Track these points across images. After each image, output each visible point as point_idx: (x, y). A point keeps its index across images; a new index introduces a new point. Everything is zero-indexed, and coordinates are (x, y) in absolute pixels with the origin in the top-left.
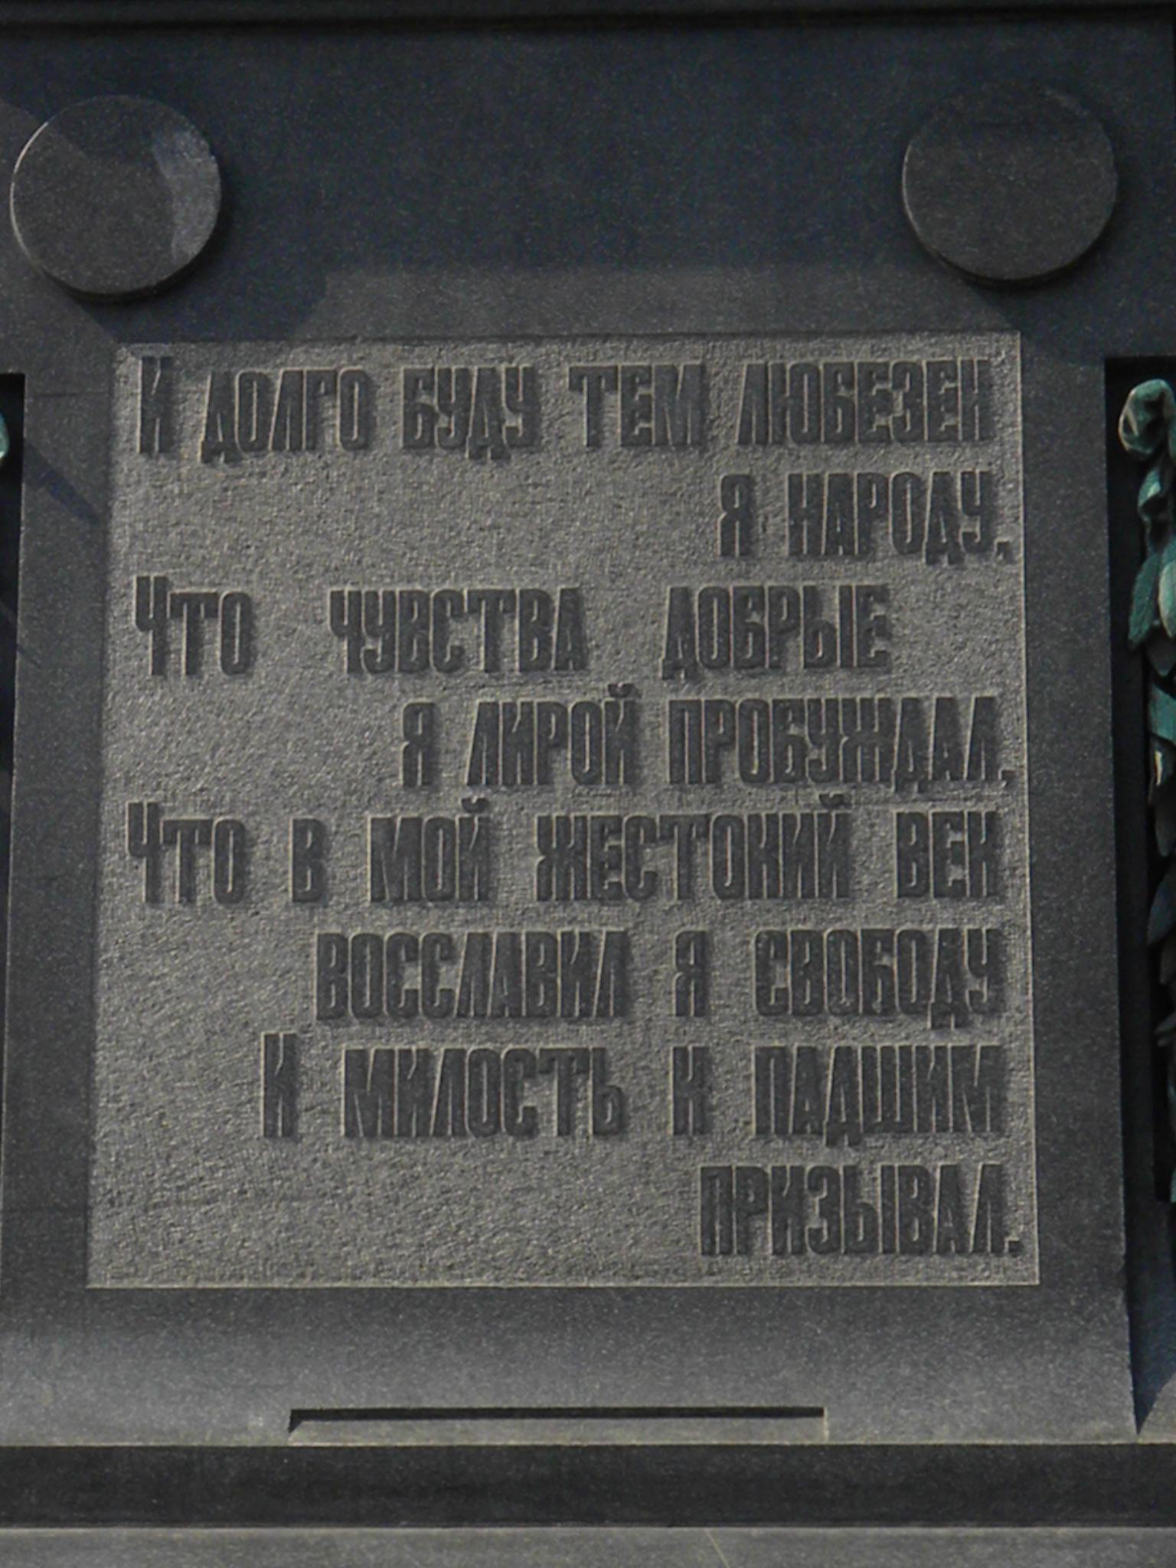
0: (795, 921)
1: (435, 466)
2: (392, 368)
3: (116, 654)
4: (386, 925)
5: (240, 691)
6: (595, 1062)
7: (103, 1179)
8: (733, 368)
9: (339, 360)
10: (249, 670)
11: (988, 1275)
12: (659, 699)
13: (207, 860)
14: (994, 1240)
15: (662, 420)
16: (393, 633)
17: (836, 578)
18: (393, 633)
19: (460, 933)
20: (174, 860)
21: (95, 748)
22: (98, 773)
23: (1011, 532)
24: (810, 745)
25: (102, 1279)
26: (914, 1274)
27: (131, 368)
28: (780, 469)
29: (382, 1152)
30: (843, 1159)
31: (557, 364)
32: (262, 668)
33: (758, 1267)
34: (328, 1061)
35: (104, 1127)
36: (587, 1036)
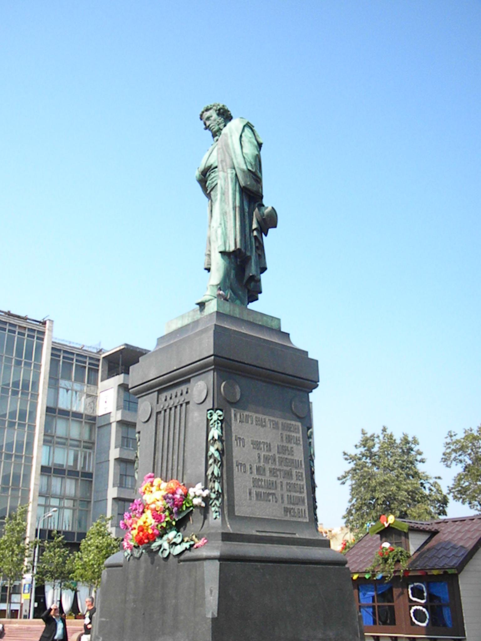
0: (289, 482)
1: (258, 427)
2: (254, 415)
3: (233, 443)
4: (257, 477)
5: (244, 449)
6: (274, 494)
7: (236, 502)
8: (280, 421)
9: (250, 414)
10: (217, 112)
11: (305, 521)
12: (277, 456)
13: (242, 468)
14: (305, 517)
15: (276, 426)
16: (256, 445)
17: (290, 446)
18: (256, 445)
19: (263, 479)
20: (239, 467)
21: (232, 454)
22: (232, 456)
23: (301, 443)
24: (26, 591)
25: (236, 514)
26: (300, 520)
27: (233, 411)
28: (285, 433)
29: (259, 502)
30: (294, 507)
31: (267, 418)
32: (246, 446)
33: (288, 518)
34: (254, 491)
35: (235, 497)
36: (273, 491)
